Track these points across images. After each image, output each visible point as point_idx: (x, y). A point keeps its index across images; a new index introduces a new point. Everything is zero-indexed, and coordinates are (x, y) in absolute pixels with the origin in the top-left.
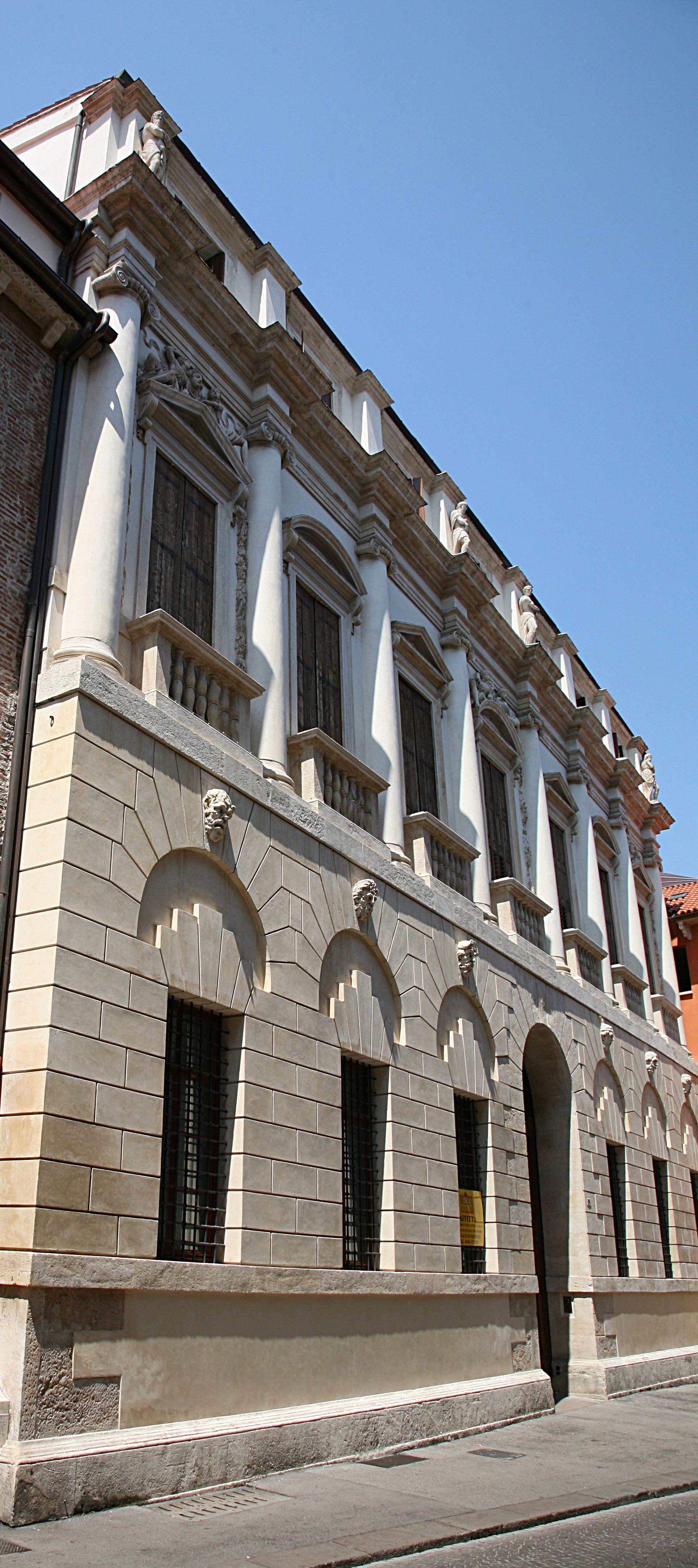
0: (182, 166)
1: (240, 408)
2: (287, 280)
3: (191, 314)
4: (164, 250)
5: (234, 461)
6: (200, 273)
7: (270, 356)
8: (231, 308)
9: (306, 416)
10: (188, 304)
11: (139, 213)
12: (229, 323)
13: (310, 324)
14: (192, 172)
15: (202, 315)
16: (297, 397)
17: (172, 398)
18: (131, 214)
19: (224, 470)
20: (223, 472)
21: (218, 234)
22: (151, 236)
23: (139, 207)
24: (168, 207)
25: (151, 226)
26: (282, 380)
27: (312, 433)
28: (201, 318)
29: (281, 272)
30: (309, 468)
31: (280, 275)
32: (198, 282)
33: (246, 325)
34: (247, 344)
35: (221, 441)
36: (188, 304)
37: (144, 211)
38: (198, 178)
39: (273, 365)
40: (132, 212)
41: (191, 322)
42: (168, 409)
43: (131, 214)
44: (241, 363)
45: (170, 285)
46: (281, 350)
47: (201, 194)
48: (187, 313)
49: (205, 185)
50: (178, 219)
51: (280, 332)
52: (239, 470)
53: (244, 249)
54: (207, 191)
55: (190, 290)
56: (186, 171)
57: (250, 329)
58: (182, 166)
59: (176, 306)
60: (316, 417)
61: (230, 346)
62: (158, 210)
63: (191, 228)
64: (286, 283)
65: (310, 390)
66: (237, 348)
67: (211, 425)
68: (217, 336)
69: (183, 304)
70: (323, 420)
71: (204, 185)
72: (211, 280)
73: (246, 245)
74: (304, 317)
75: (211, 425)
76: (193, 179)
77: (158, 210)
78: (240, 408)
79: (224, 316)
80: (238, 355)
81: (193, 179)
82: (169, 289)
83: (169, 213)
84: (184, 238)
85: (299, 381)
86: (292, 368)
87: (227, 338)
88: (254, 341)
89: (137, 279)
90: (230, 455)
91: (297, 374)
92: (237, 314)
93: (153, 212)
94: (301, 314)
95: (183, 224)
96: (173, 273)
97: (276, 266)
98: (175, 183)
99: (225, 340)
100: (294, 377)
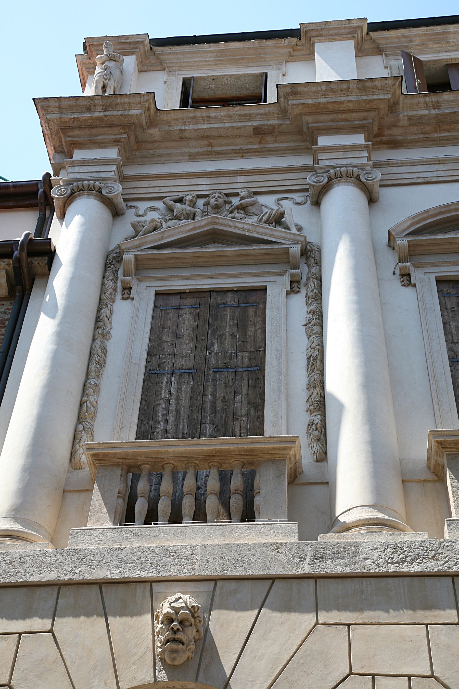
0: (177, 54)
1: (450, 173)
2: (348, 31)
3: (198, 154)
4: (119, 136)
5: (272, 236)
6: (177, 120)
7: (301, 115)
8: (230, 116)
9: (404, 122)
10: (187, 150)
11: (76, 132)
12: (238, 128)
13: (415, 36)
14: (187, 48)
15: (210, 145)
16: (365, 119)
17: (162, 239)
18: (70, 139)
19: (263, 252)
20: (265, 254)
21: (251, 64)
22: (99, 137)
23: (73, 128)
24: (95, 106)
25: (94, 131)
26: (332, 121)
27: (427, 129)
28: (209, 149)
29: (336, 31)
30: (439, 161)
31: (336, 35)
32: (179, 128)
33: (257, 114)
34: (274, 127)
35: (249, 230)
36: (187, 150)
37: (80, 127)
38: (197, 47)
39: (309, 119)
40: (70, 137)
41: (204, 160)
42: (155, 252)
43: (70, 139)
44: (285, 145)
45: (158, 152)
46: (302, 101)
47: (209, 55)
48: (193, 157)
49: (206, 45)
50: (110, 106)
51: (288, 90)
52: (285, 238)
53: (287, 50)
54: (212, 47)
55: (182, 139)
56: (182, 53)
57: (265, 114)
58: (177, 54)
59: (178, 162)
60: (414, 113)
61: (260, 143)
62: (87, 115)
63: (127, 100)
64: (349, 33)
65: (371, 101)
66: (269, 138)
67: (230, 226)
68: (238, 147)
69: (182, 154)
70: (427, 108)
71: (206, 47)
72: (191, 115)
73: (286, 47)
74: (404, 37)
75: (230, 226)
76: (194, 52)
77: (87, 115)
78: (450, 173)
79: (228, 128)
80: (275, 142)
81: (194, 52)
82: (159, 156)
83: (99, 108)
84: (126, 112)
85: (351, 106)
86: (329, 103)
87: (251, 140)
88: (278, 119)
89: (78, 180)
90: (265, 234)
91: (341, 103)
92: (240, 116)
93: (85, 120)
94: (398, 38)
95: (117, 104)
96: (155, 141)
97: (324, 33)
98: (180, 70)
99: (251, 143)
100: (343, 107)
